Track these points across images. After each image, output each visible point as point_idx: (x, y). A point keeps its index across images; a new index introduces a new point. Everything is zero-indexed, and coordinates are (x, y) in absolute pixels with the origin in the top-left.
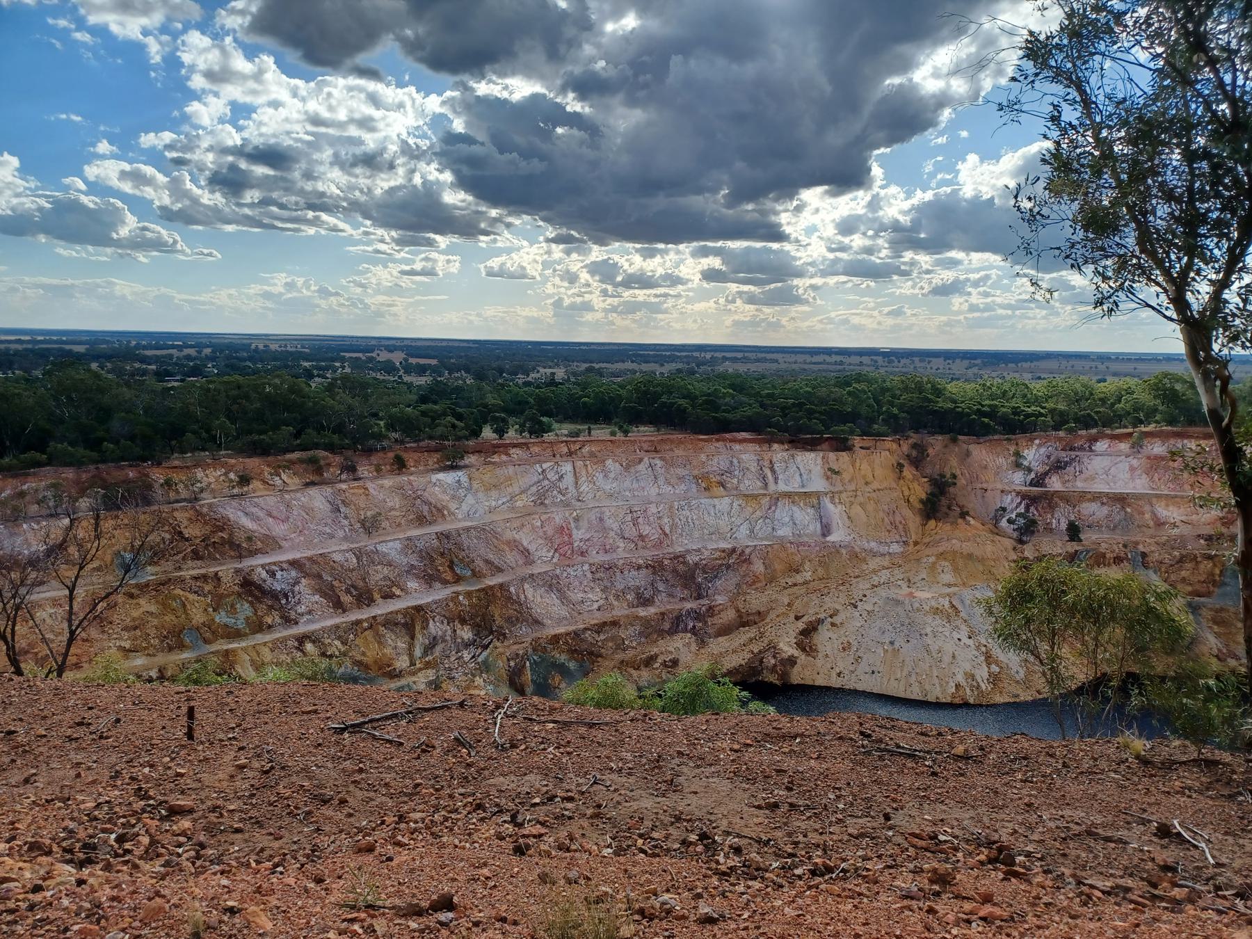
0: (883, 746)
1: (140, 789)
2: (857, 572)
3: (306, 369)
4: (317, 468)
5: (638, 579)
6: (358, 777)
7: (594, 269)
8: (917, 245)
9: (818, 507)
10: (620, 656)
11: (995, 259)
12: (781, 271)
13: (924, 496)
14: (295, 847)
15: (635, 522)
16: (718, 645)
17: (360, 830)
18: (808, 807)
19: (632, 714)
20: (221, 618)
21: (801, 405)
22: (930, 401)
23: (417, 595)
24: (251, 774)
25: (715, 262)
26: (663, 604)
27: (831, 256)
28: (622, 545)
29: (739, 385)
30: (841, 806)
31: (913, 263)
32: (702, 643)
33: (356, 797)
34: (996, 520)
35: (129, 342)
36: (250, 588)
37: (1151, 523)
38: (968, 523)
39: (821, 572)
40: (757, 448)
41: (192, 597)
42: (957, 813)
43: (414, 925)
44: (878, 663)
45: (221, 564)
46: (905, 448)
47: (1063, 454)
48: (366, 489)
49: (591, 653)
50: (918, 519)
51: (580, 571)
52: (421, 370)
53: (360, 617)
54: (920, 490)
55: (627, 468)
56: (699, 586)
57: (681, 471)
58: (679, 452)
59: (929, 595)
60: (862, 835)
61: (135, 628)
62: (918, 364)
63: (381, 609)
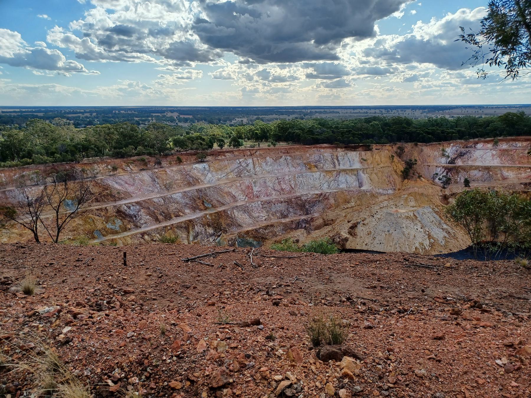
0: (415, 264)
1: (110, 284)
2: (374, 202)
3: (137, 121)
4: (144, 163)
5: (282, 207)
6: (198, 278)
7: (259, 74)
8: (398, 61)
9: (357, 175)
10: (275, 239)
11: (431, 65)
12: (338, 72)
13: (403, 169)
14: (180, 305)
15: (279, 183)
16: (316, 234)
17: (205, 298)
18: (388, 288)
19: (305, 254)
20: (109, 226)
21: (350, 131)
22: (405, 128)
23: (190, 215)
24: (153, 278)
25: (310, 70)
26: (292, 217)
27: (362, 66)
28: (274, 193)
29: (323, 124)
30: (402, 287)
31: (396, 69)
32: (309, 233)
33: (200, 286)
34: (434, 178)
35: (61, 111)
36: (120, 213)
37: (501, 179)
38: (422, 180)
39: (358, 202)
40: (331, 150)
41: (97, 217)
42: (452, 289)
43: (249, 330)
44: (383, 240)
45: (107, 204)
46: (395, 149)
47: (463, 150)
48: (166, 171)
49: (263, 238)
50: (400, 179)
51: (256, 204)
52: (186, 120)
53: (167, 225)
54: (401, 167)
55: (275, 161)
56: (307, 210)
57: (298, 161)
58: (298, 153)
59: (404, 211)
60: (414, 298)
61: (74, 231)
62: (400, 112)
63: (175, 221)
